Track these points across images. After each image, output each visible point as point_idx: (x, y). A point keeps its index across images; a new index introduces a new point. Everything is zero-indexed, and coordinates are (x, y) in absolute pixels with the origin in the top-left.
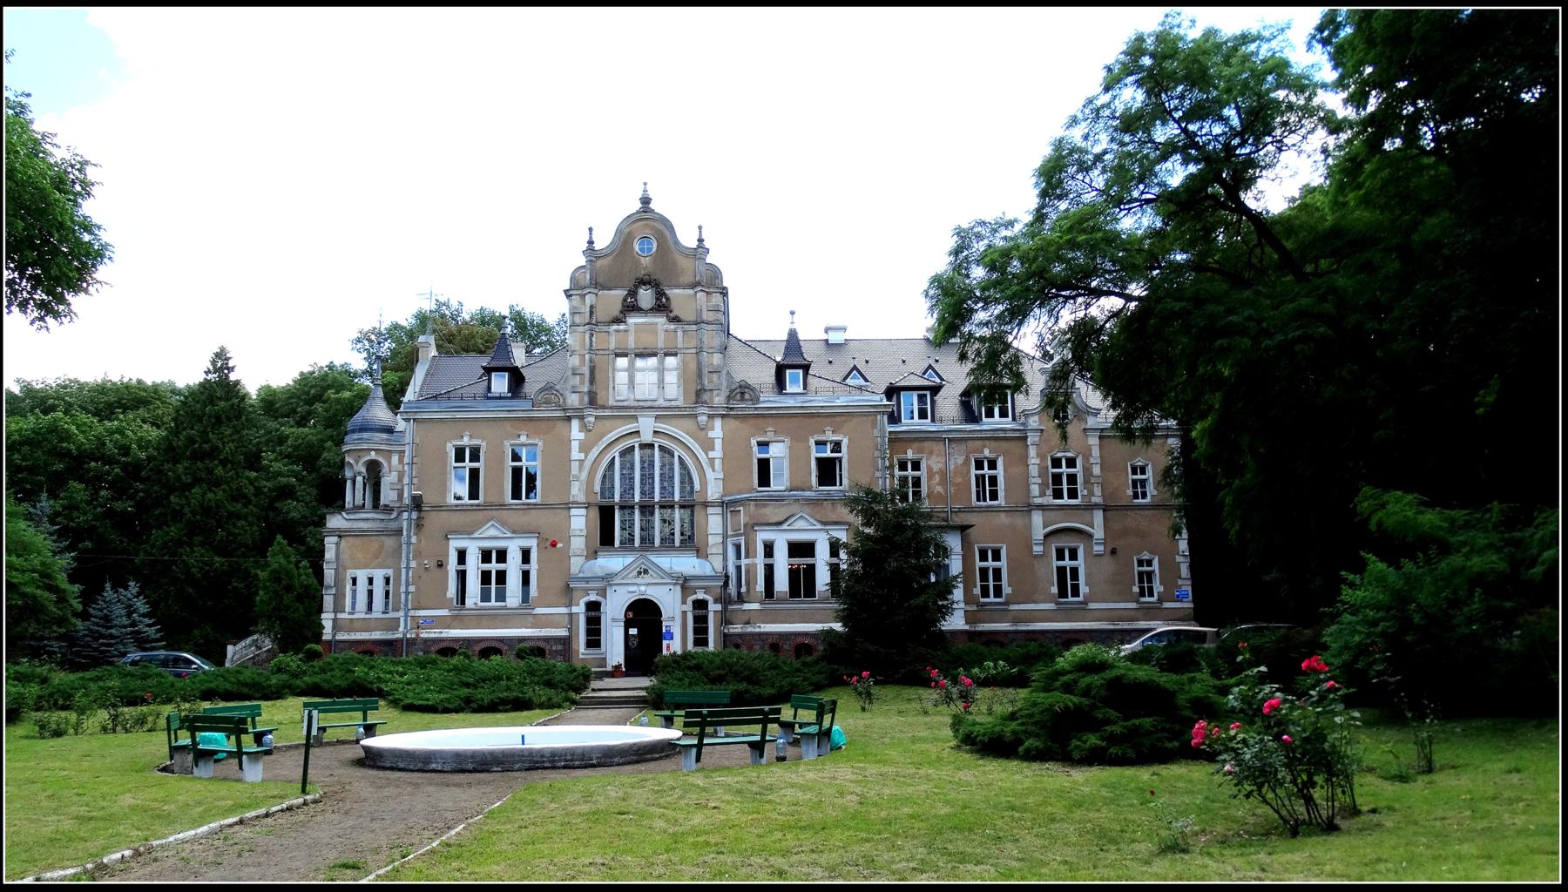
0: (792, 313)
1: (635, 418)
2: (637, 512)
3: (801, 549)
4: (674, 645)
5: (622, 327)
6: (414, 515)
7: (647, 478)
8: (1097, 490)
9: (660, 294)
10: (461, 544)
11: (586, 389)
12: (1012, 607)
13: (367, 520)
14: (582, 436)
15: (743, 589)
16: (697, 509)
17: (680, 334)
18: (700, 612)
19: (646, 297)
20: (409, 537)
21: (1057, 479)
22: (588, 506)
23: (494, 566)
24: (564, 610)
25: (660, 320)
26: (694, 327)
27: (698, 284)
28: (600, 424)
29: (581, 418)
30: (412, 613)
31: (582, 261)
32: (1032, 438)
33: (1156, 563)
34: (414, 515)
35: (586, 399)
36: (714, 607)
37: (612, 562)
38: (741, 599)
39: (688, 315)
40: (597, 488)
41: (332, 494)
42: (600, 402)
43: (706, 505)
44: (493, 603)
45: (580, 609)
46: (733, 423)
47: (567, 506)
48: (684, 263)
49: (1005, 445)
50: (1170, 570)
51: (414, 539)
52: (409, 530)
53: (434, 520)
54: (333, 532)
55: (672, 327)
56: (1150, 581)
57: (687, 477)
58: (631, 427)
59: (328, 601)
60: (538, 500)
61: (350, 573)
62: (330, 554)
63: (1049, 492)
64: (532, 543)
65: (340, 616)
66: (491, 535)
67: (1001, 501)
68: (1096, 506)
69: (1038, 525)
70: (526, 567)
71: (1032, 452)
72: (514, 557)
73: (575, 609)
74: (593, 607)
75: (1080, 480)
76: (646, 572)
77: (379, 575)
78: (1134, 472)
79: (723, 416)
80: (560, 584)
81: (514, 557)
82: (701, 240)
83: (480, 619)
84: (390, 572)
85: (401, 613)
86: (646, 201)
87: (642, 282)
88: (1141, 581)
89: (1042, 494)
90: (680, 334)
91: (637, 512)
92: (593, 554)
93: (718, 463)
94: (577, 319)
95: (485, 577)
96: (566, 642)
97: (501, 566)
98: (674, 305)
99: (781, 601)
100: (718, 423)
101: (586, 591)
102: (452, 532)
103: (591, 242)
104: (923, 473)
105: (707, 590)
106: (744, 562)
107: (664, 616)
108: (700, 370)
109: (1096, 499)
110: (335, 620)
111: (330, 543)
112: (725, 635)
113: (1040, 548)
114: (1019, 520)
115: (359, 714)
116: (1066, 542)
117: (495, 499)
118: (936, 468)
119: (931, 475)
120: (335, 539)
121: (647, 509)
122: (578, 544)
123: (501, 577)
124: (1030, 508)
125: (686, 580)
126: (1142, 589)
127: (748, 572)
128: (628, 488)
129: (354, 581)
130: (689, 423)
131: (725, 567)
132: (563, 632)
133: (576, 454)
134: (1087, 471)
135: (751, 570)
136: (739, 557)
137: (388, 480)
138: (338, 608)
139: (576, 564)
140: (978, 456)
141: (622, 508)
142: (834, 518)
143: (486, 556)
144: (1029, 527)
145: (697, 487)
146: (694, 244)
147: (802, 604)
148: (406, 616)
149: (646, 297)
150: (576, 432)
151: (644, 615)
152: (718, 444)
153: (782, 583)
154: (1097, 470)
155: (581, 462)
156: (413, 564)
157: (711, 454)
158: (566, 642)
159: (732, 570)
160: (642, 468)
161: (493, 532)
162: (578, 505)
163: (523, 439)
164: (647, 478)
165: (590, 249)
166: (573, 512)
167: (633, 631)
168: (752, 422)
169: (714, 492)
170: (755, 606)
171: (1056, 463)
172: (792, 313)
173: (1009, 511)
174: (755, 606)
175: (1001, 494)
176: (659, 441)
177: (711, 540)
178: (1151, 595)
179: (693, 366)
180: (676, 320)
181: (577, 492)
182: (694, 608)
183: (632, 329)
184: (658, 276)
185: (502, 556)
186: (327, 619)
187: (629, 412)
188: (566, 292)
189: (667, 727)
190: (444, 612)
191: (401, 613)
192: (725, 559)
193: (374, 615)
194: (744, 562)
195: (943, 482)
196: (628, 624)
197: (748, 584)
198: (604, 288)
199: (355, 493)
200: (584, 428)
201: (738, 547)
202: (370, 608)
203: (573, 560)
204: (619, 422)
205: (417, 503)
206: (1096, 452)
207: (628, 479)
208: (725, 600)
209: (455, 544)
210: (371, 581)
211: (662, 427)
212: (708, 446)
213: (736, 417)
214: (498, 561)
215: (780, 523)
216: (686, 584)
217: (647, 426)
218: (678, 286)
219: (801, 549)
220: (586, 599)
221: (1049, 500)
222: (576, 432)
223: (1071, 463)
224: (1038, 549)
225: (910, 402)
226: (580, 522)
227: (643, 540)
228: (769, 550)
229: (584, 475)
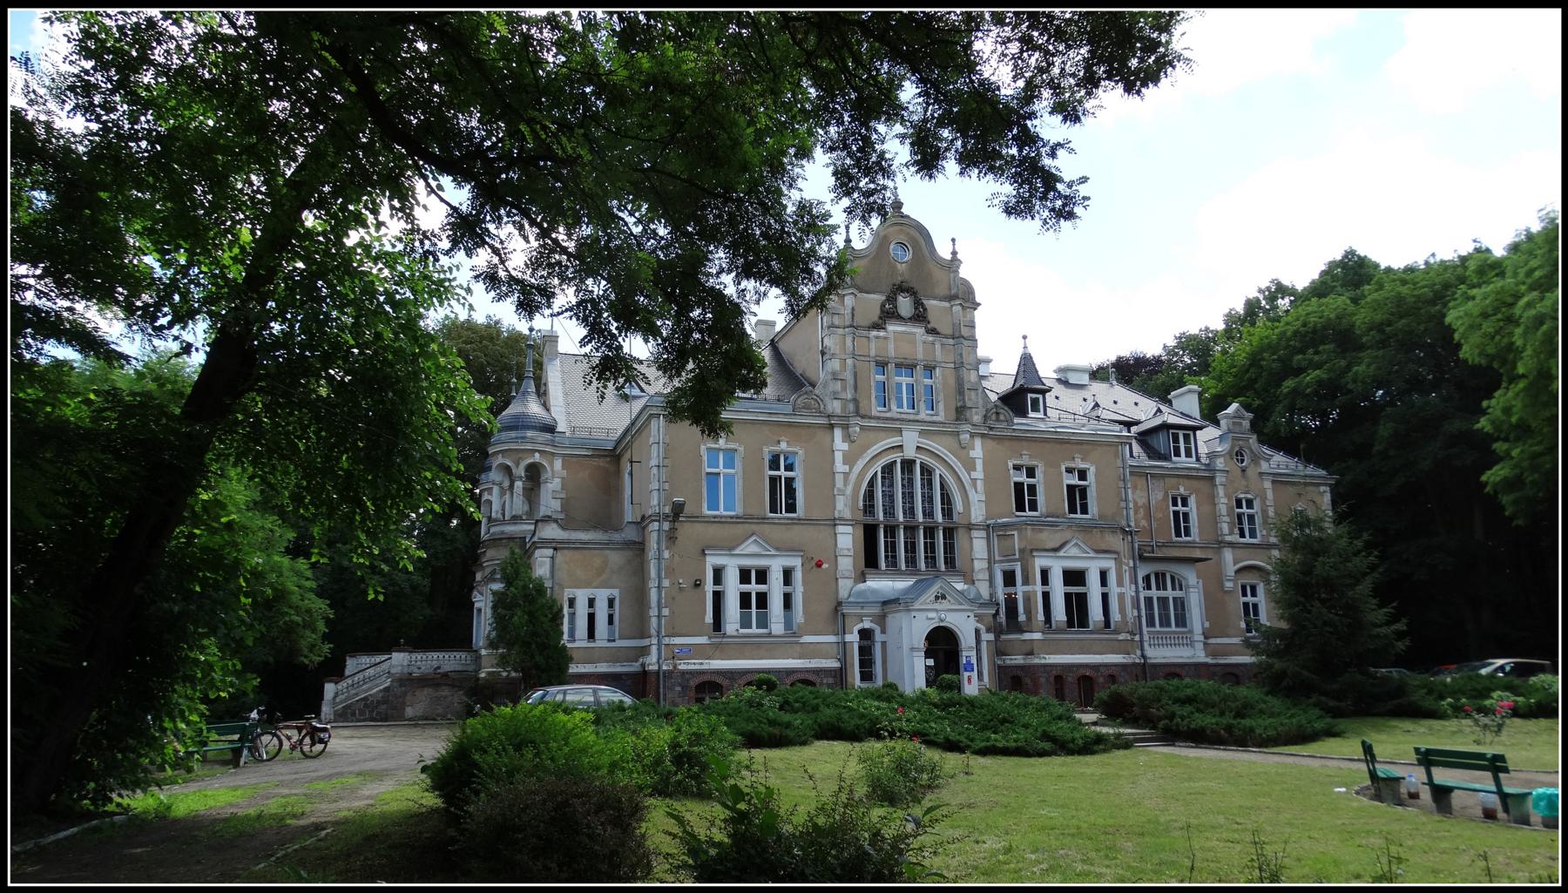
0: (1025, 337)
1: (900, 431)
3: (1074, 577)
5: (882, 334)
7: (909, 496)
9: (918, 304)
14: (845, 446)
17: (938, 346)
19: (905, 304)
23: (754, 588)
25: (919, 331)
26: (951, 341)
29: (846, 427)
30: (666, 640)
32: (1220, 479)
34: (666, 526)
35: (851, 407)
39: (945, 328)
42: (862, 412)
43: (970, 527)
44: (754, 630)
45: (853, 638)
47: (834, 522)
48: (938, 274)
49: (1195, 483)
51: (666, 554)
53: (686, 531)
54: (545, 543)
57: (947, 500)
60: (739, 511)
63: (1236, 531)
64: (796, 562)
66: (751, 553)
70: (1046, 589)
71: (1221, 491)
72: (776, 578)
74: (865, 634)
76: (944, 597)
77: (602, 596)
79: (983, 436)
80: (827, 607)
81: (776, 578)
82: (954, 253)
87: (901, 288)
88: (1247, 613)
89: (1231, 533)
90: (938, 346)
95: (745, 599)
96: (840, 675)
97: (762, 588)
98: (931, 316)
100: (978, 442)
101: (860, 618)
102: (709, 547)
112: (1000, 667)
116: (1249, 579)
117: (754, 511)
120: (550, 552)
122: (846, 564)
123: (763, 600)
124: (1221, 544)
128: (889, 511)
130: (950, 440)
132: (834, 664)
133: (840, 467)
134: (1264, 512)
135: (1028, 599)
139: (845, 586)
142: (1104, 547)
143: (745, 576)
144: (1220, 565)
145: (958, 506)
146: (948, 257)
147: (1076, 635)
148: (659, 644)
149: (905, 304)
150: (840, 444)
151: (942, 645)
152: (979, 465)
153: (1059, 612)
154: (1271, 512)
155: (846, 475)
156: (666, 583)
158: (840, 675)
161: (753, 549)
163: (783, 446)
164: (909, 496)
166: (840, 529)
168: (1007, 443)
169: (978, 514)
170: (1037, 636)
172: (1025, 337)
174: (1037, 636)
175: (1194, 530)
176: (921, 458)
177: (978, 565)
179: (952, 381)
180: (932, 331)
181: (842, 507)
183: (891, 336)
184: (917, 286)
185: (762, 576)
190: (703, 640)
191: (654, 641)
195: (1149, 516)
200: (847, 437)
202: (591, 634)
204: (882, 434)
206: (1270, 494)
207: (889, 498)
209: (712, 560)
210: (591, 602)
211: (927, 443)
212: (970, 465)
213: (994, 438)
214: (757, 582)
215: (1056, 550)
217: (910, 441)
218: (935, 298)
219: (1074, 577)
220: (860, 626)
221: (1236, 538)
223: (1250, 504)
224: (1229, 585)
226: (847, 539)
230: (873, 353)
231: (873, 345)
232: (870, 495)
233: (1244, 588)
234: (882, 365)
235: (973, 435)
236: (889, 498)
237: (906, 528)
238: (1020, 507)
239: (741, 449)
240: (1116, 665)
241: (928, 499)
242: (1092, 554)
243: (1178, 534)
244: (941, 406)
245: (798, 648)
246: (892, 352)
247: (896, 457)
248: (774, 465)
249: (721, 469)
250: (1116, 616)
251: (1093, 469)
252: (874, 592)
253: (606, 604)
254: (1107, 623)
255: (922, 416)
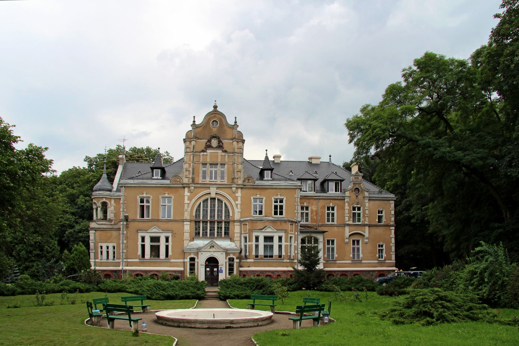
1: (209, 188)
2: (216, 224)
4: (222, 277)
5: (205, 153)
6: (125, 223)
7: (213, 211)
8: (367, 219)
9: (220, 142)
10: (143, 234)
11: (191, 176)
12: (338, 262)
13: (104, 225)
14: (189, 194)
15: (247, 254)
16: (231, 224)
17: (227, 156)
18: (192, 262)
19: (214, 143)
20: (123, 231)
21: (354, 214)
22: (191, 221)
24: (182, 261)
25: (220, 152)
26: (232, 154)
27: (235, 138)
28: (196, 190)
29: (189, 187)
31: (191, 128)
33: (384, 246)
35: (191, 180)
36: (236, 260)
37: (200, 243)
38: (246, 257)
40: (194, 214)
41: (87, 214)
42: (196, 182)
43: (234, 221)
45: (187, 260)
46: (245, 191)
47: (183, 221)
50: (389, 249)
52: (123, 229)
53: (132, 225)
54: (93, 229)
55: (224, 154)
56: (382, 253)
57: (227, 211)
58: (207, 191)
59: (92, 255)
60: (150, 218)
61: (100, 244)
62: (92, 237)
63: (351, 219)
64: (169, 235)
65: (97, 260)
67: (335, 223)
68: (366, 225)
69: (347, 231)
70: (167, 244)
71: (346, 204)
73: (186, 260)
74: (192, 259)
75: (361, 215)
76: (213, 247)
77: (111, 245)
78: (379, 213)
79: (241, 188)
82: (236, 122)
83: (149, 264)
84: (115, 244)
85: (121, 260)
86: (215, 107)
88: (379, 253)
89: (349, 220)
90: (227, 156)
91: (216, 224)
92: (192, 239)
93: (239, 206)
94: (188, 150)
99: (261, 259)
100: (239, 190)
101: (190, 253)
102: (140, 230)
103: (194, 122)
104: (309, 211)
105: (234, 254)
106: (289, 244)
107: (220, 264)
108: (234, 170)
109: (366, 223)
110: (95, 262)
111: (92, 233)
112: (240, 271)
113: (347, 240)
114: (341, 229)
115: (140, 302)
116: (356, 238)
118: (314, 209)
119: (312, 211)
120: (94, 232)
121: (219, 222)
122: (187, 236)
125: (227, 250)
126: (379, 255)
127: (249, 247)
129: (101, 247)
130: (229, 190)
131: (241, 245)
132: (182, 269)
133: (186, 201)
135: (251, 246)
136: (246, 242)
137: (111, 209)
138: (96, 257)
139: (186, 243)
140: (328, 205)
141: (203, 222)
144: (344, 232)
145: (231, 215)
146: (233, 124)
147: (268, 260)
148: (123, 261)
149: (214, 143)
150: (187, 193)
151: (212, 262)
152: (239, 199)
153: (261, 252)
155: (188, 204)
157: (237, 202)
158: (182, 272)
159: (243, 247)
160: (211, 207)
161: (155, 230)
162: (187, 220)
164: (213, 211)
165: (194, 125)
167: (208, 269)
169: (237, 217)
170: (252, 260)
171: (354, 209)
173: (337, 226)
175: (335, 220)
177: (236, 235)
178: (382, 258)
179: (231, 169)
180: (225, 151)
181: (187, 216)
182: (190, 260)
183: (209, 154)
186: (92, 261)
187: (206, 186)
188: (184, 139)
189: (252, 309)
190: (137, 260)
192: (241, 242)
193: (110, 261)
194: (248, 243)
196: (206, 267)
197: (249, 252)
198: (198, 138)
199: (98, 214)
200: (189, 191)
201: (246, 238)
203: (185, 241)
204: (203, 189)
205: (126, 219)
207: (205, 211)
208: (240, 258)
210: (108, 247)
215: (262, 229)
216: (227, 252)
217: (213, 191)
218: (227, 139)
222: (187, 193)
223: (359, 209)
224: (347, 240)
225: (332, 185)
226: (187, 227)
227: (210, 234)
228: (257, 238)
229: (189, 209)
230: (201, 160)
231: (201, 157)
232: (198, 210)
233: (354, 241)
234: (204, 164)
235: (237, 188)
236: (205, 211)
237: (225, 222)
238: (276, 213)
239: (151, 197)
240: (281, 271)
241: (220, 211)
242: (275, 231)
243: (328, 221)
244: (226, 178)
245: (169, 263)
246: (208, 160)
247: (208, 197)
248: (142, 201)
249: (167, 204)
250: (283, 253)
251: (264, 198)
252: (196, 244)
253: (106, 248)
254: (280, 256)
255: (219, 182)
